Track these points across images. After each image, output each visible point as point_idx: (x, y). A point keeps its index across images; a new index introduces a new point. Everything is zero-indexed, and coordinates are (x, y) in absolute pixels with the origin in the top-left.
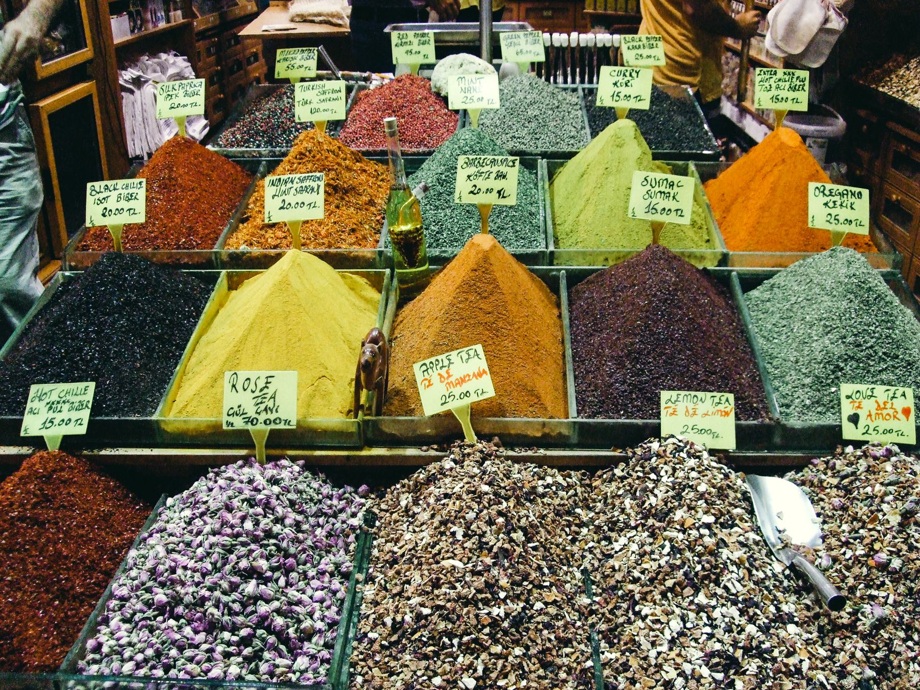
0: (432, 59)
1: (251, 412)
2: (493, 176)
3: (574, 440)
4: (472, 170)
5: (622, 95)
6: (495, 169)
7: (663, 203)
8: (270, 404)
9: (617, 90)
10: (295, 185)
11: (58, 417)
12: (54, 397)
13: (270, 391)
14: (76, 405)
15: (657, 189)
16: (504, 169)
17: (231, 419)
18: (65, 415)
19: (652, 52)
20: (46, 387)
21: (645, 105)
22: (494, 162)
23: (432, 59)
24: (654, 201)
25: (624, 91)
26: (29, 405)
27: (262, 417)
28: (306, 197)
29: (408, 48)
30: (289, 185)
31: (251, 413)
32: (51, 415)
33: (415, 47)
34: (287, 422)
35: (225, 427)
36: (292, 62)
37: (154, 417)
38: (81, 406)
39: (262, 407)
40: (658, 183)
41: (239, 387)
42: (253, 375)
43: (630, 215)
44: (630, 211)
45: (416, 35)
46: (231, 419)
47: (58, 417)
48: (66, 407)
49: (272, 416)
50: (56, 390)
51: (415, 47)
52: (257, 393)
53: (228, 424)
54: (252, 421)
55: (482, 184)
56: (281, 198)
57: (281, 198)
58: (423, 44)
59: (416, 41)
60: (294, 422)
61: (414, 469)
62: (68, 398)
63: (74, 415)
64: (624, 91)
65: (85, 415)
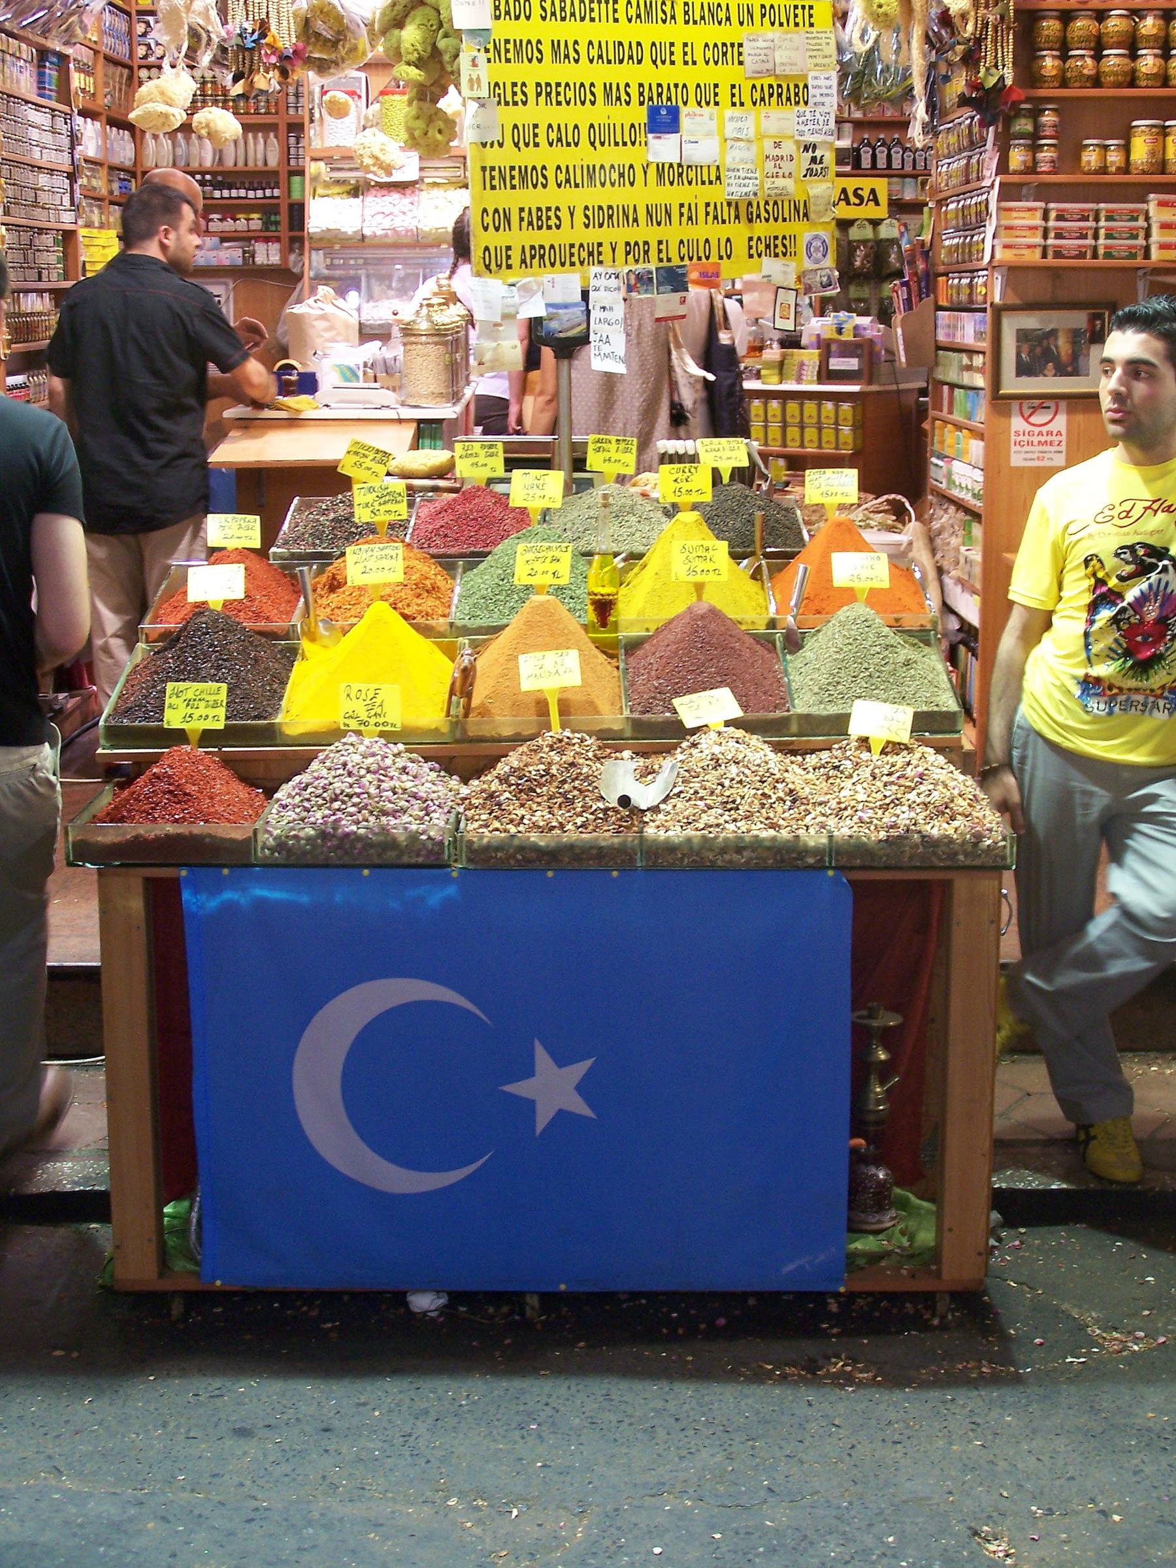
0: (500, 472)
1: (364, 716)
2: (549, 560)
3: (628, 734)
4: (531, 556)
5: (683, 490)
6: (550, 554)
7: (701, 565)
8: (379, 711)
9: (679, 486)
10: (375, 553)
11: (197, 713)
12: (190, 695)
13: (378, 701)
14: (211, 703)
15: (695, 554)
16: (557, 554)
17: (347, 721)
18: (202, 711)
19: (733, 454)
20: (182, 685)
21: (708, 498)
22: (549, 548)
23: (500, 472)
24: (693, 565)
25: (686, 486)
26: (167, 702)
27: (373, 721)
28: (386, 563)
29: (475, 460)
30: (370, 553)
31: (364, 717)
32: (189, 711)
33: (482, 460)
34: (393, 725)
35: (342, 727)
36: (362, 460)
37: (277, 721)
38: (215, 705)
39: (373, 712)
40: (695, 549)
41: (353, 696)
42: (364, 687)
43: (673, 579)
44: (673, 574)
45: (483, 447)
46: (347, 721)
47: (197, 713)
48: (202, 704)
49: (381, 720)
50: (191, 688)
51: (482, 460)
52: (368, 702)
53: (345, 725)
54: (364, 723)
55: (538, 567)
56: (363, 565)
57: (363, 565)
58: (491, 456)
59: (482, 453)
60: (399, 725)
61: (497, 759)
62: (203, 696)
63: (211, 712)
64: (686, 486)
65: (222, 712)
